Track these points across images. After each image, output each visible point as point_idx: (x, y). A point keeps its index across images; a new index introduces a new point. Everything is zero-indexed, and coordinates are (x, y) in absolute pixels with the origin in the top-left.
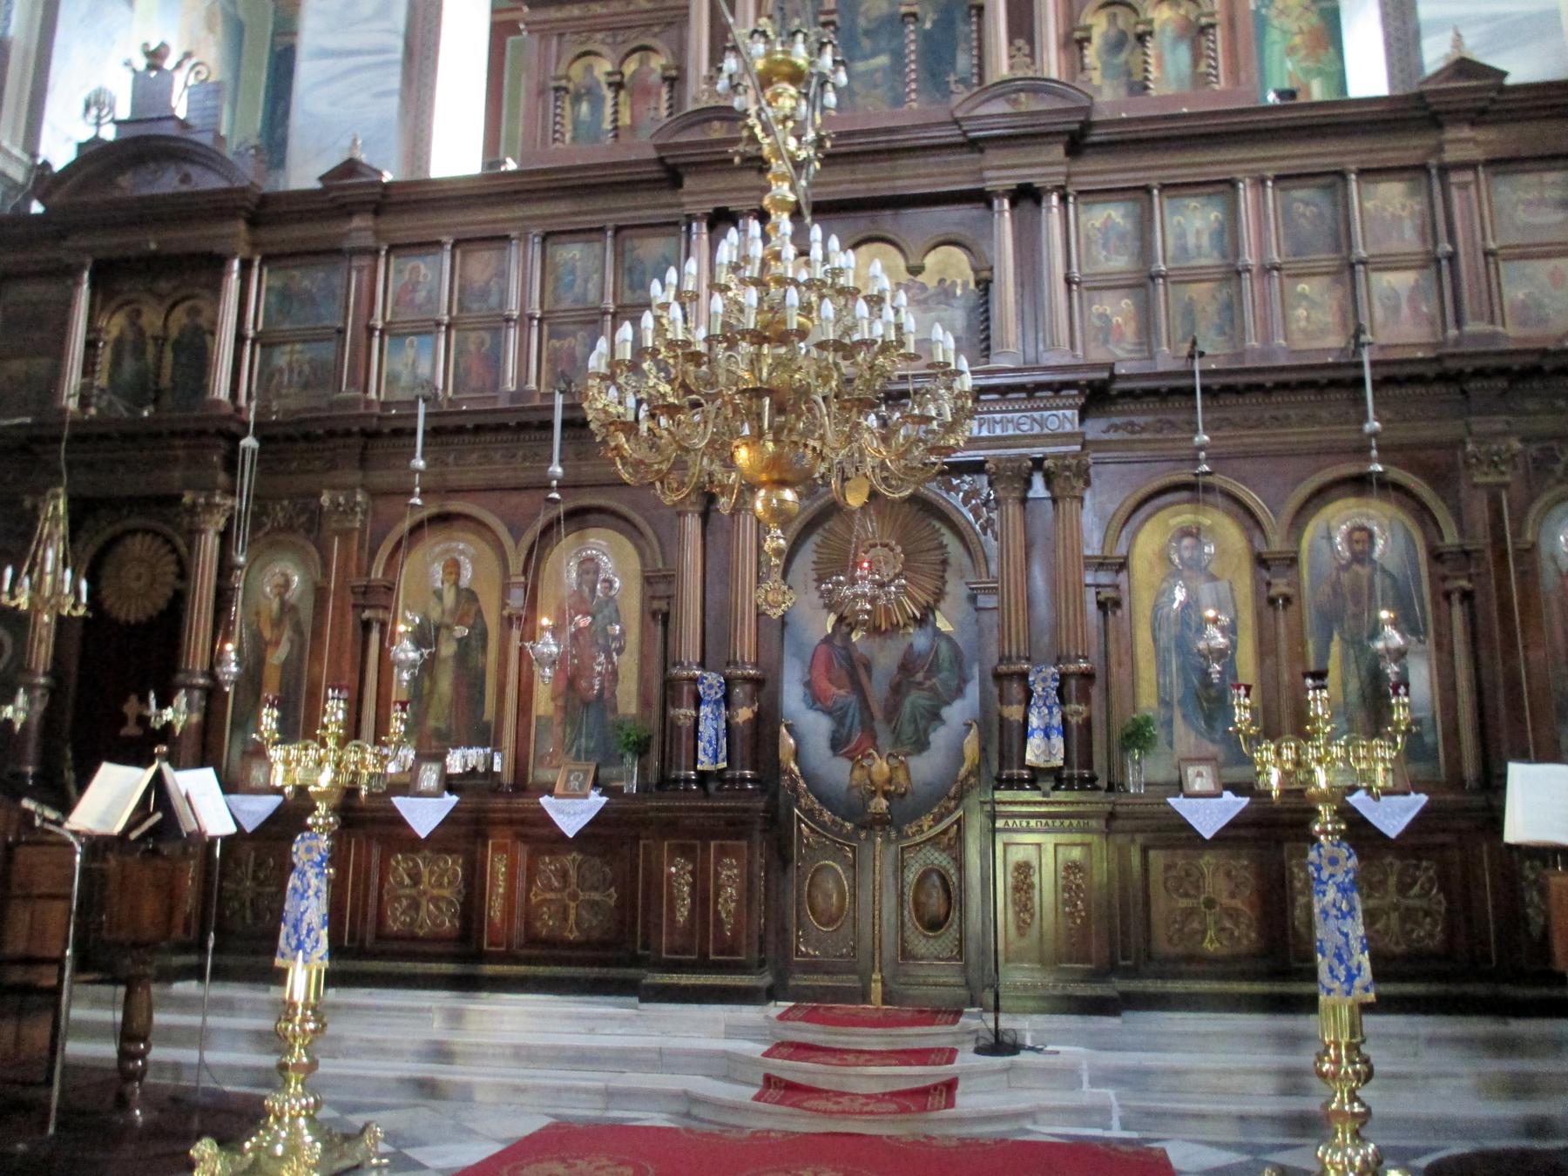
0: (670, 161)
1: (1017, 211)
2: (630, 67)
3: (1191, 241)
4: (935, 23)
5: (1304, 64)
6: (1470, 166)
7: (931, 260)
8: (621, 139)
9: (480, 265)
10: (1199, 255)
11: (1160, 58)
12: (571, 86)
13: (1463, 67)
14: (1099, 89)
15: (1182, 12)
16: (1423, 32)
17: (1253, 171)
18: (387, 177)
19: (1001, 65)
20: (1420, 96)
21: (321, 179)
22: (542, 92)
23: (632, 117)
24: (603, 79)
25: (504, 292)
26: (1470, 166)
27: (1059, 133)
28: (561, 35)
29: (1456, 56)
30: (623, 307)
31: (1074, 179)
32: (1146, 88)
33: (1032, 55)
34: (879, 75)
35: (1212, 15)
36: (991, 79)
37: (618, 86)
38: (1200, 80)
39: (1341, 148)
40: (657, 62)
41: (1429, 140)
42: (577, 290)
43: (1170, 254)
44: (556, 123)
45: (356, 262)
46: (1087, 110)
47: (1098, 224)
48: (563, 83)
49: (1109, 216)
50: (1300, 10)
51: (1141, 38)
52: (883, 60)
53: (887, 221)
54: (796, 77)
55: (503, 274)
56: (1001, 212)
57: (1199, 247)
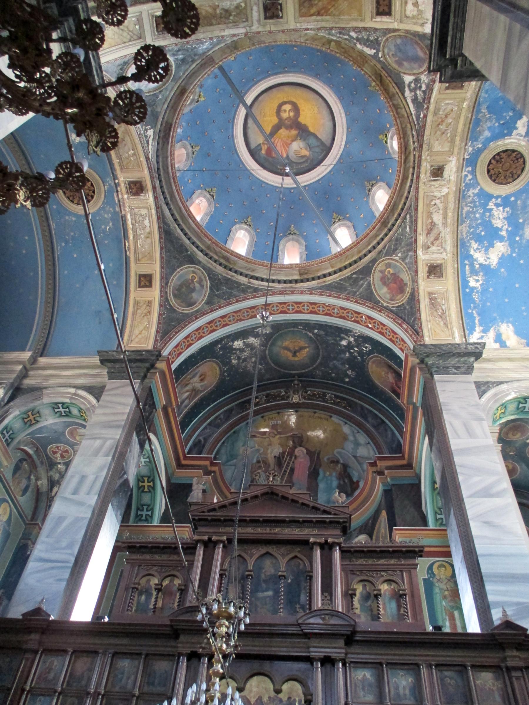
0: (175, 627)
1: (323, 668)
2: (166, 582)
3: (401, 691)
4: (292, 580)
5: (450, 604)
6: (520, 669)
7: (285, 687)
8: (156, 613)
9: (81, 665)
10: (406, 699)
11: (384, 605)
12: (140, 587)
13: (508, 624)
14: (359, 616)
15: (392, 587)
16: (491, 607)
17: (427, 661)
18: (52, 618)
19: (318, 601)
20: (493, 635)
21: (23, 615)
22: (127, 589)
23: (162, 604)
24: (153, 586)
25: (90, 679)
26: (520, 669)
27: (343, 635)
28: (140, 566)
29: (505, 619)
30: (143, 693)
31: (349, 656)
32: (379, 618)
33: (331, 600)
34: (268, 599)
35: (404, 590)
36: (314, 608)
37: (159, 590)
38: (401, 617)
39: (463, 654)
40: (177, 582)
41: (500, 655)
42: (123, 682)
43: (392, 696)
44: (131, 599)
45: (27, 656)
46: (354, 626)
47: (359, 678)
48: (136, 586)
49: (365, 675)
50: (446, 580)
51: (376, 596)
52: (270, 593)
53: (267, 666)
54: (229, 617)
55: (91, 670)
56: (317, 668)
57: (405, 695)
